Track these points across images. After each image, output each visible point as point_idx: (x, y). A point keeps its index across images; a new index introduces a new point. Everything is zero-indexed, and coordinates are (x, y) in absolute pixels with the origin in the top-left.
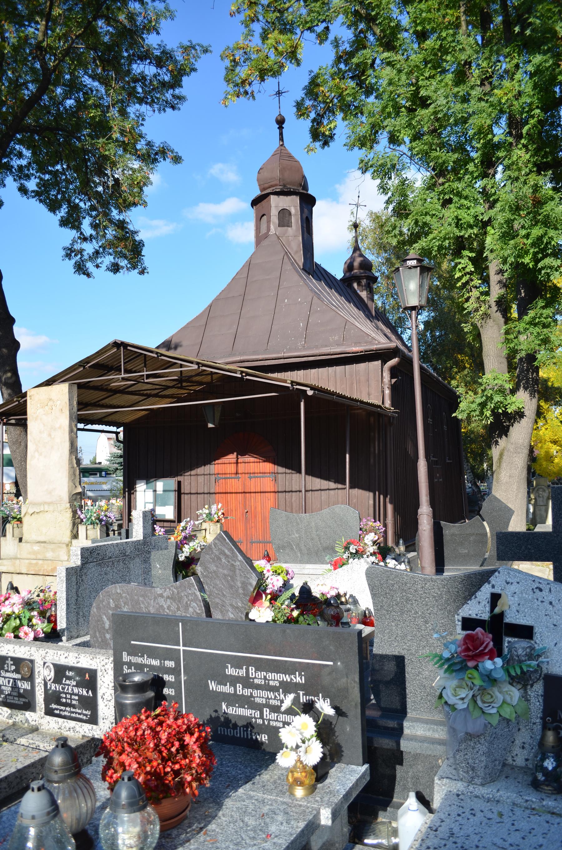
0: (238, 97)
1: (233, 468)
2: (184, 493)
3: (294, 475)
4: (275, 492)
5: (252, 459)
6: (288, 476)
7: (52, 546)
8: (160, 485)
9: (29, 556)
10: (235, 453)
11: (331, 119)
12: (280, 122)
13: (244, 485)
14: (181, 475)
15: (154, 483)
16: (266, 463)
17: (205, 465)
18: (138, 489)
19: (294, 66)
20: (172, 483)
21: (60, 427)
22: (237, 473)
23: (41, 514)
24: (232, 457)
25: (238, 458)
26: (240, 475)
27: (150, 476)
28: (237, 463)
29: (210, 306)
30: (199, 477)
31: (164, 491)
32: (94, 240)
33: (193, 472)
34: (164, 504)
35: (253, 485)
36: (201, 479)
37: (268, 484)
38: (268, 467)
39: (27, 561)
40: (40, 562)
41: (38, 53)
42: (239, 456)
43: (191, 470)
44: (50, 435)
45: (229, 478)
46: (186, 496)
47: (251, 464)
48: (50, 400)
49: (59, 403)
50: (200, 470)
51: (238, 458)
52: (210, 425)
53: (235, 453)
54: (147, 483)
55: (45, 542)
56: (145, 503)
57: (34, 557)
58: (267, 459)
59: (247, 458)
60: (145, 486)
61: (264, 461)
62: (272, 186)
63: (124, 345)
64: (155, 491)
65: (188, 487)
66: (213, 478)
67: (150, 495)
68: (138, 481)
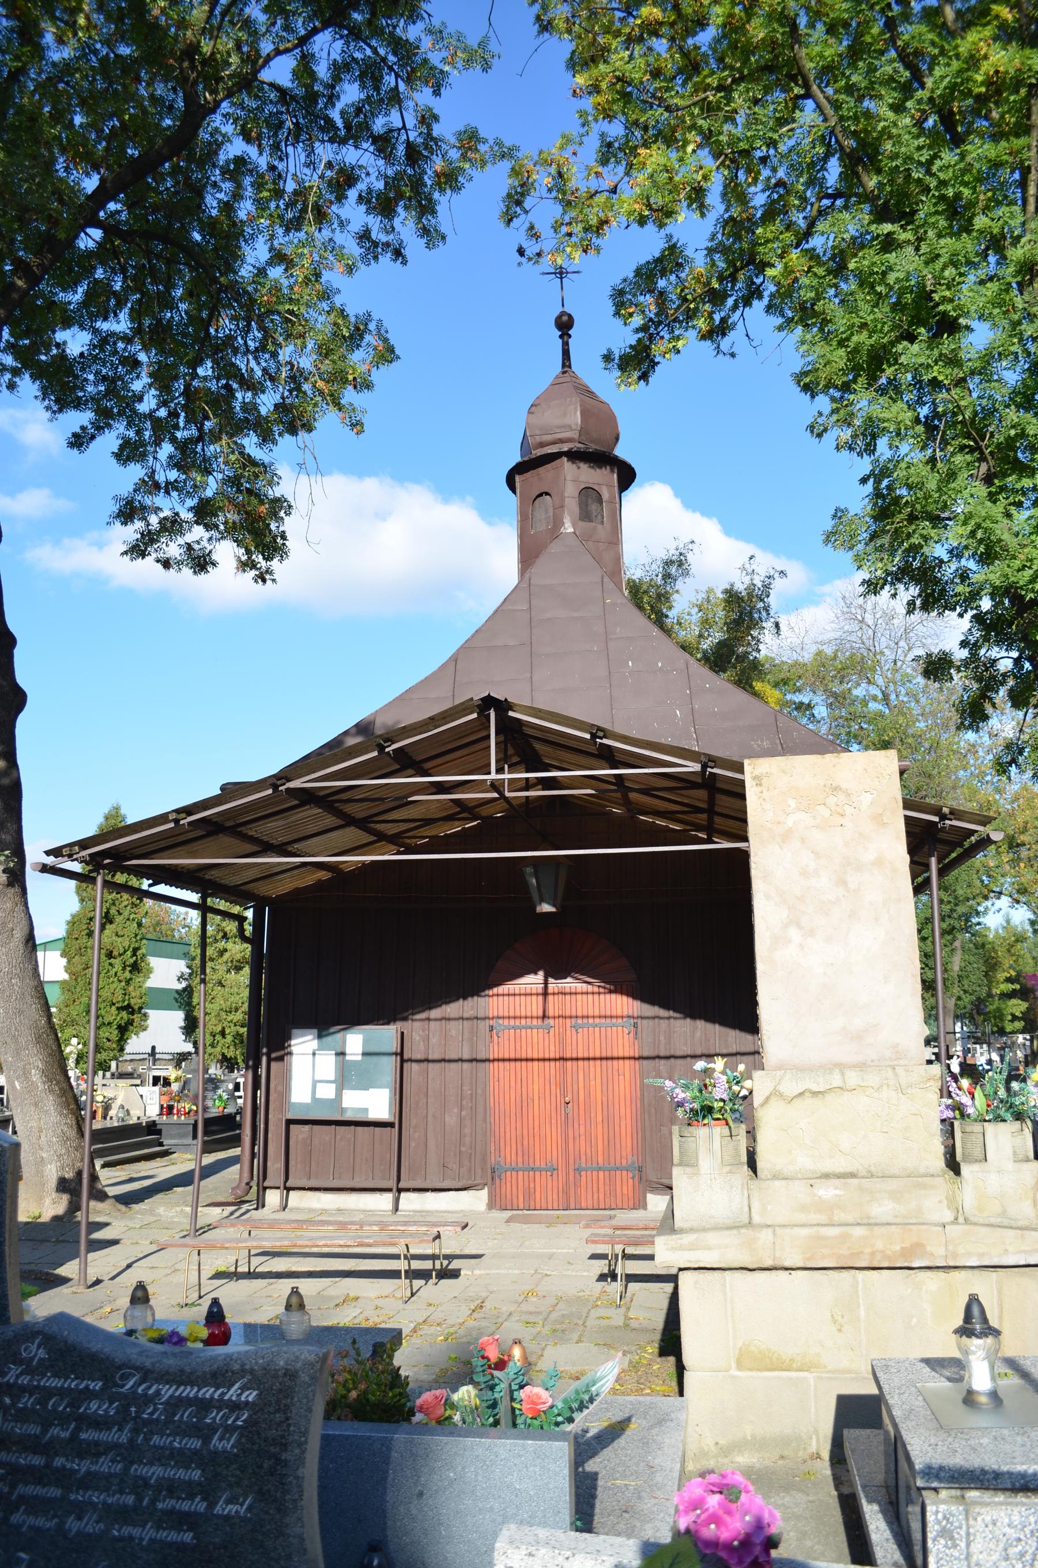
0: (585, 251)
1: (535, 1005)
2: (410, 1060)
3: (680, 1023)
4: (634, 1058)
5: (581, 987)
6: (664, 1023)
7: (893, 1185)
8: (355, 1041)
9: (802, 1218)
10: (541, 973)
11: (677, 333)
12: (564, 325)
13: (562, 1042)
14: (405, 1019)
15: (339, 1036)
16: (613, 996)
17: (465, 998)
18: (294, 1049)
19: (696, 216)
20: (386, 1035)
21: (879, 862)
22: (544, 1016)
23: (829, 1097)
24: (533, 981)
25: (546, 983)
26: (551, 1022)
27: (327, 1020)
28: (545, 994)
29: (455, 659)
30: (432, 1023)
31: (365, 1054)
32: (174, 494)
33: (435, 1013)
34: (365, 1084)
35: (580, 1043)
36: (454, 1027)
37: (623, 1043)
38: (622, 1004)
39: (805, 1232)
40: (859, 1232)
41: (186, 64)
42: (551, 980)
43: (430, 1008)
44: (842, 883)
45: (526, 1028)
46: (415, 1066)
47: (580, 995)
48: (836, 789)
49: (867, 798)
50: (452, 1009)
51: (546, 983)
52: (546, 908)
53: (541, 973)
54: (320, 1036)
55: (852, 1175)
56: (315, 1083)
57: (822, 1218)
58: (619, 988)
59: (569, 983)
60: (315, 1044)
61: (611, 992)
62: (561, 441)
63: (502, 706)
64: (341, 1054)
65: (422, 1047)
66: (484, 1025)
67: (327, 1064)
68: (295, 1031)
